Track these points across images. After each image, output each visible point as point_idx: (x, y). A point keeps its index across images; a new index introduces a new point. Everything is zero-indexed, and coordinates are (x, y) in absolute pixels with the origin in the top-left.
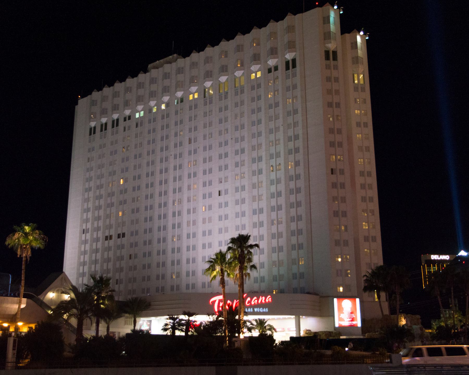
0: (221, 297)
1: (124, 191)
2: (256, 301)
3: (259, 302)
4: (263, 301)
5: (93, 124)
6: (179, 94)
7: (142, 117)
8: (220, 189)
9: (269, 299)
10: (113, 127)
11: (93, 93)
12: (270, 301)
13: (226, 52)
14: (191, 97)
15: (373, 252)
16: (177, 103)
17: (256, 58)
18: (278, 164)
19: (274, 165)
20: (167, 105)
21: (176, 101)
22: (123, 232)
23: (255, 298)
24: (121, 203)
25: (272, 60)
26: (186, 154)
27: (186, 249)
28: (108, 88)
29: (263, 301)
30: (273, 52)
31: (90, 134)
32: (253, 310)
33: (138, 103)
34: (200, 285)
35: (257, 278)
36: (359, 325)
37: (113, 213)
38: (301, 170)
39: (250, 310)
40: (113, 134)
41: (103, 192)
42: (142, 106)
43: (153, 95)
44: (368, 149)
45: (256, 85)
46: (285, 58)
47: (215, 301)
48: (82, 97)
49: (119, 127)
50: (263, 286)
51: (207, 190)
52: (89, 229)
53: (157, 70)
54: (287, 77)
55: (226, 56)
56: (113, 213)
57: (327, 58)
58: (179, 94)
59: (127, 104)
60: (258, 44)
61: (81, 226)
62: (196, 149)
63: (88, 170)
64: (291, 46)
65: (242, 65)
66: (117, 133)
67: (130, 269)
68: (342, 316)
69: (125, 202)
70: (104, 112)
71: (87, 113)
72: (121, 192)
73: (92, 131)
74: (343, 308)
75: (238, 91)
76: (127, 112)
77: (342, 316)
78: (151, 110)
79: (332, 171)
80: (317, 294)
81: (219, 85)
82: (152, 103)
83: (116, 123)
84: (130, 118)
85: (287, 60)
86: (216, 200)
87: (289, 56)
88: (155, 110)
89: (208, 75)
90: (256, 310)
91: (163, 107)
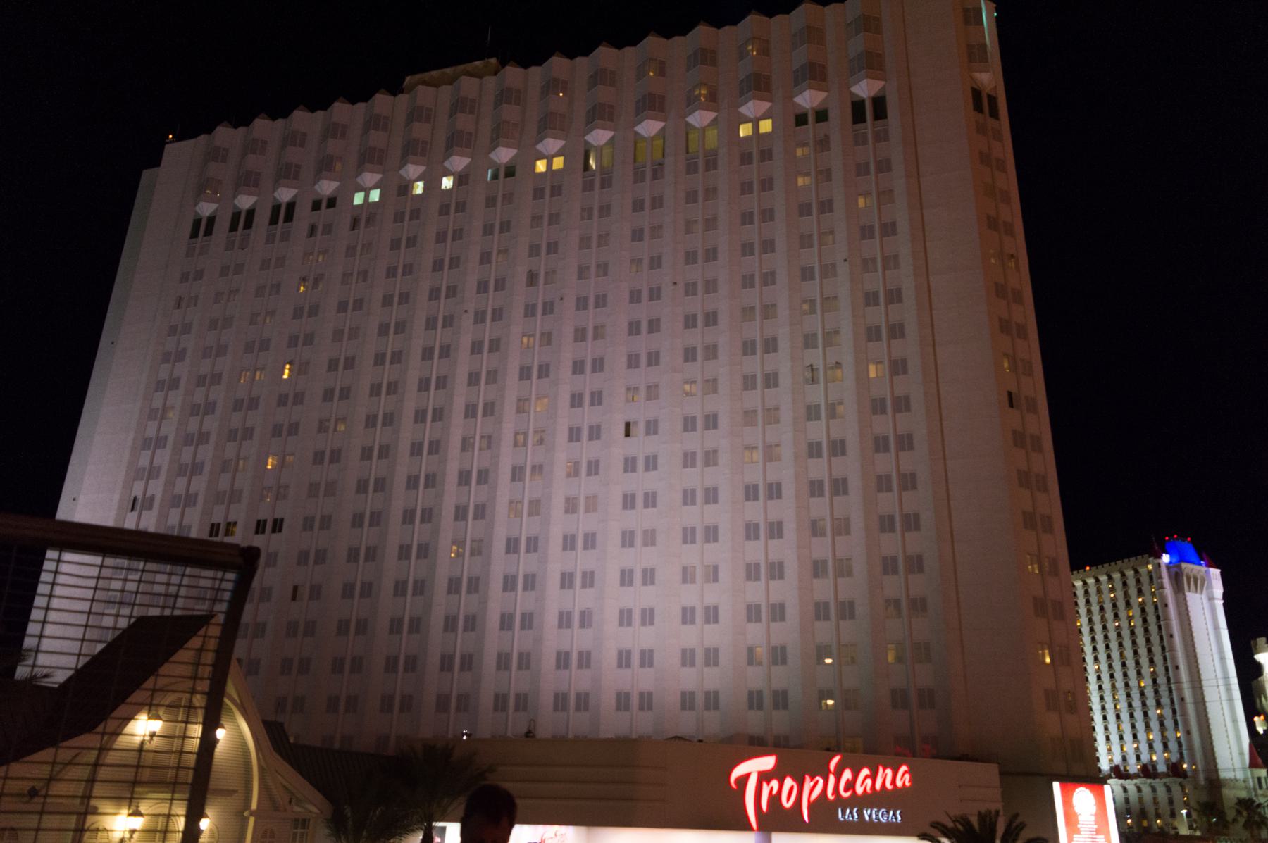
0: (768, 763)
1: (291, 398)
2: (869, 782)
3: (878, 786)
5: (206, 209)
6: (504, 155)
7: (558, 171)
8: (631, 419)
10: (233, 228)
11: (219, 129)
12: (907, 784)
13: (662, 63)
14: (358, 199)
16: (495, 177)
17: (759, 85)
18: (831, 362)
20: (461, 180)
21: (490, 171)
22: (278, 515)
24: (277, 431)
25: (814, 92)
26: (518, 312)
27: (500, 585)
28: (231, 131)
29: (889, 786)
30: (814, 74)
31: (194, 234)
33: (411, 157)
34: (547, 699)
35: (760, 693)
37: (246, 459)
38: (912, 384)
39: (850, 815)
40: (270, 239)
41: (218, 394)
42: (378, 177)
43: (413, 150)
45: (762, 148)
46: (852, 94)
47: (744, 779)
48: (178, 138)
49: (253, 231)
50: (780, 722)
51: (587, 416)
52: (152, 498)
53: (476, 80)
54: (860, 140)
55: (662, 72)
56: (246, 459)
57: (978, 107)
58: (504, 155)
59: (325, 166)
60: (765, 51)
61: (128, 485)
62: (552, 303)
63: (172, 330)
64: (872, 63)
65: (713, 97)
66: (285, 237)
67: (292, 630)
69: (294, 429)
70: (248, 181)
71: (179, 185)
72: (282, 400)
73: (203, 228)
74: (1075, 815)
75: (643, 172)
76: (327, 187)
78: (406, 188)
79: (1011, 400)
81: (635, 143)
82: (412, 170)
83: (284, 214)
84: (332, 202)
85: (799, 112)
86: (617, 448)
87: (864, 89)
88: (419, 188)
89: (600, 114)
91: (447, 183)
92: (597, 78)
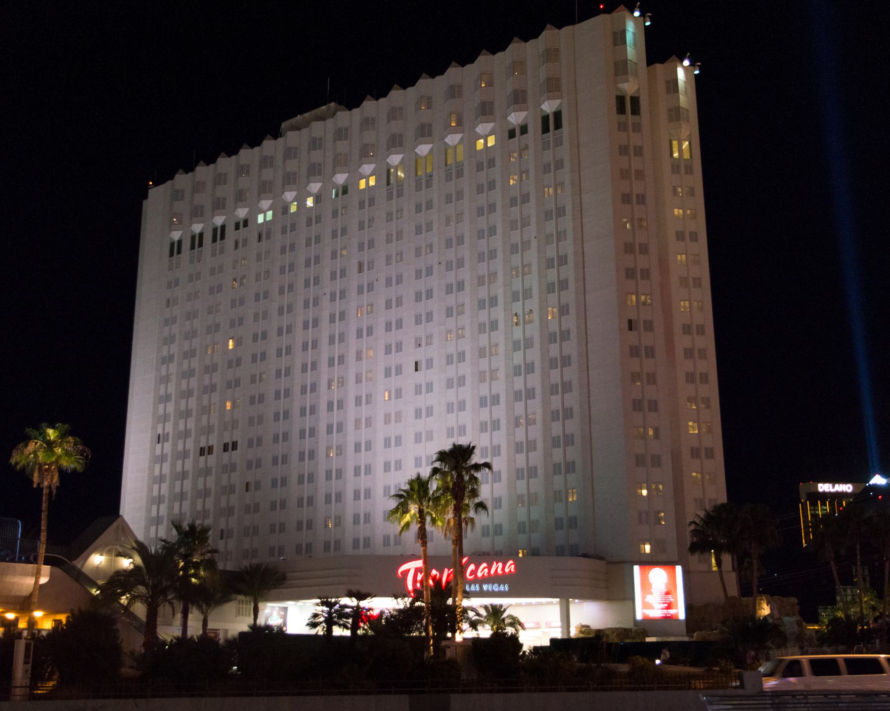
0: (419, 563)
1: (235, 362)
2: (486, 570)
3: (492, 572)
4: (499, 571)
5: (176, 235)
6: (341, 178)
7: (270, 221)
8: (418, 359)
9: (510, 567)
10: (214, 240)
11: (177, 176)
12: (512, 570)
13: (429, 98)
14: (362, 184)
15: (707, 477)
16: (337, 195)
17: (486, 110)
18: (527, 310)
19: (520, 313)
20: (318, 199)
21: (334, 191)
22: (234, 440)
23: (485, 565)
24: (229, 385)
25: (517, 113)
26: (353, 292)
27: (353, 473)
28: (205, 168)
29: (499, 571)
30: (519, 99)
31: (171, 254)
32: (481, 587)
33: (263, 195)
34: (379, 540)
35: (488, 527)
36: (682, 616)
37: (214, 404)
38: (570, 322)
39: (475, 588)
40: (214, 254)
41: (195, 363)
42: (270, 202)
43: (290, 180)
44: (698, 282)
45: (486, 161)
46: (542, 110)
47: (408, 571)
48: (156, 184)
49: (226, 240)
50: (500, 542)
51: (394, 359)
52: (168, 434)
53: (297, 132)
54: (546, 146)
55: (429, 107)
56: (214, 404)
57: (621, 110)
58: (341, 178)
59: (240, 197)
60: (490, 84)
61: (154, 428)
62: (372, 283)
63: (167, 322)
64: (552, 87)
65: (459, 123)
66: (222, 251)
67: (247, 509)
68: (649, 599)
69: (237, 383)
70: (197, 213)
71: (166, 215)
72: (230, 365)
73: (175, 248)
74: (650, 585)
75: (451, 173)
76: (242, 213)
77: (649, 599)
78: (286, 209)
79: (631, 325)
80: (601, 558)
81: (416, 161)
82: (289, 196)
83: (219, 234)
84: (246, 223)
85: (545, 114)
86: (410, 379)
87: (548, 107)
88: (293, 208)
89: (396, 142)
90: (485, 587)
91: (310, 202)
92: (551, 55)
